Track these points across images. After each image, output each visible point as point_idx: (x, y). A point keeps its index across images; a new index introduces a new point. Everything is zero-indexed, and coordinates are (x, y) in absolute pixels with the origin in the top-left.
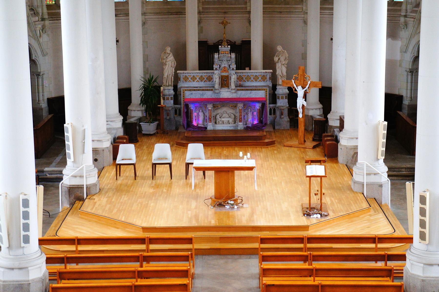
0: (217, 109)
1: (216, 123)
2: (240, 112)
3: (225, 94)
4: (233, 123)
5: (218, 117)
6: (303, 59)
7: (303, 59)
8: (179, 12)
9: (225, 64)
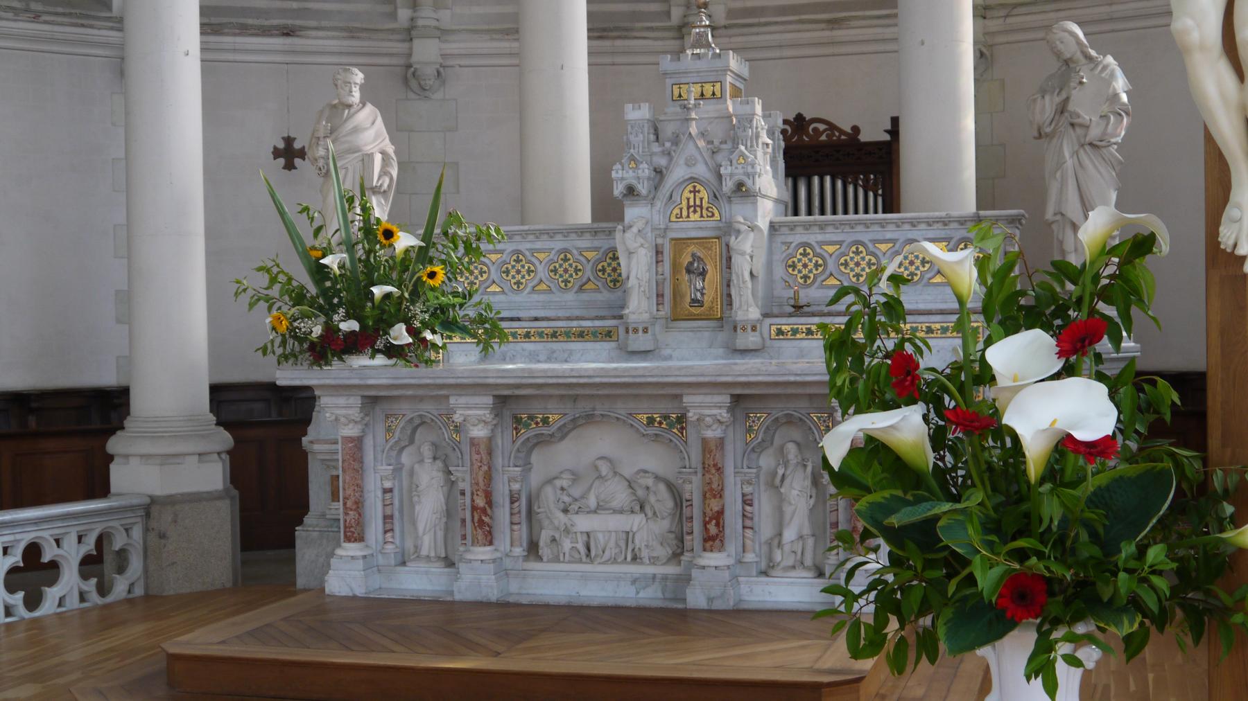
0: (541, 441)
1: (533, 549)
3: (592, 362)
4: (663, 552)
8: (616, 29)
9: (690, 163)
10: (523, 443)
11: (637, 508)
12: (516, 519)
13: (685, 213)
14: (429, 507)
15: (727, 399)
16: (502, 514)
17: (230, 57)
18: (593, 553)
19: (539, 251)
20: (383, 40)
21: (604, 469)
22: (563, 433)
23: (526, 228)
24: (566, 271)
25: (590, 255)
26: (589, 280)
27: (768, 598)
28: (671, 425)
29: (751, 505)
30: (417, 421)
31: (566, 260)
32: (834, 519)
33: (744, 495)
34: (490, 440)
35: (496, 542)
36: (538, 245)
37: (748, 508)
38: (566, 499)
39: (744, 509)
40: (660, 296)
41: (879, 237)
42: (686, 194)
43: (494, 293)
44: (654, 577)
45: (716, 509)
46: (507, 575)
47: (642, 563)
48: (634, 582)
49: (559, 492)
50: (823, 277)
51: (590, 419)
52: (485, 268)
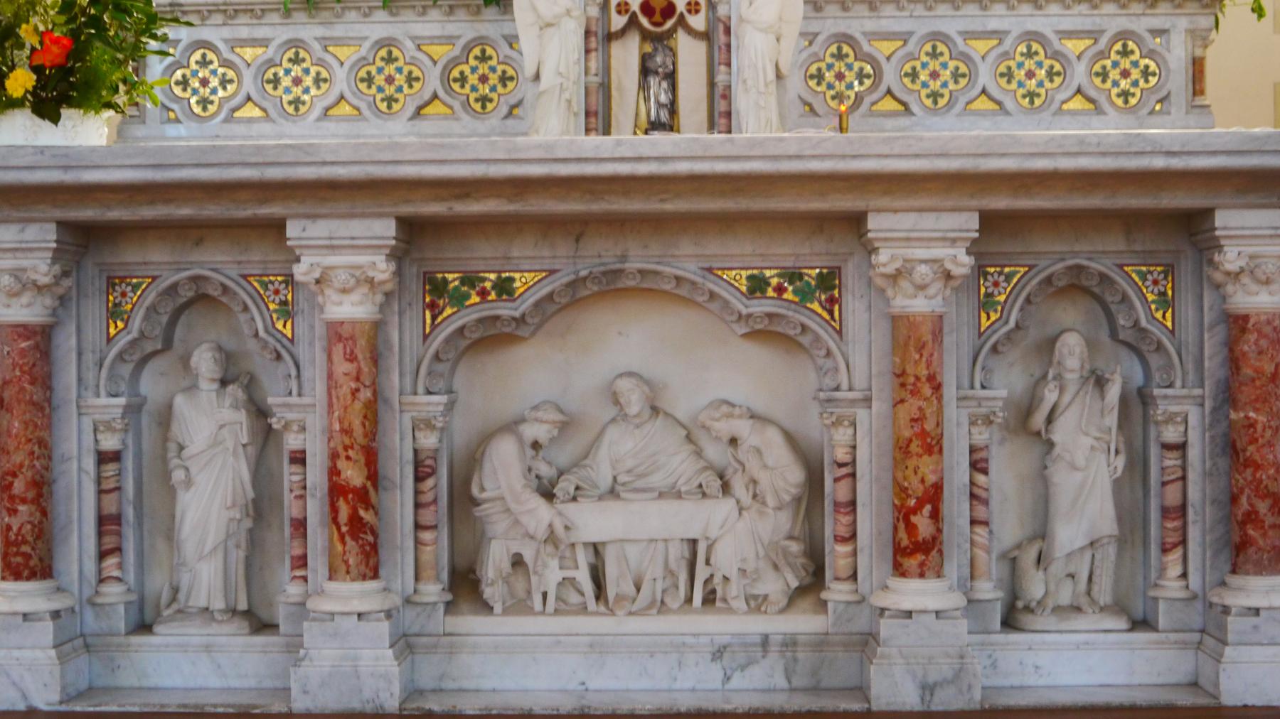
0: (493, 338)
1: (465, 585)
2: (914, 378)
4: (774, 586)
5: (504, 471)
6: (910, 617)
7: (910, 617)
10: (447, 341)
12: (427, 516)
14: (208, 499)
15: (973, 221)
16: (398, 506)
18: (611, 592)
19: (339, 42)
22: (549, 309)
24: (390, 80)
25: (439, 51)
26: (435, 96)
27: (1031, 680)
28: (805, 295)
29: (985, 472)
30: (187, 293)
31: (390, 59)
32: (1172, 496)
33: (973, 450)
34: (377, 327)
35: (382, 572)
37: (981, 479)
39: (972, 483)
41: (976, 25)
43: (250, 120)
44: (765, 641)
45: (931, 478)
47: (730, 611)
48: (719, 654)
50: (875, 96)
51: (610, 287)
52: (231, 74)
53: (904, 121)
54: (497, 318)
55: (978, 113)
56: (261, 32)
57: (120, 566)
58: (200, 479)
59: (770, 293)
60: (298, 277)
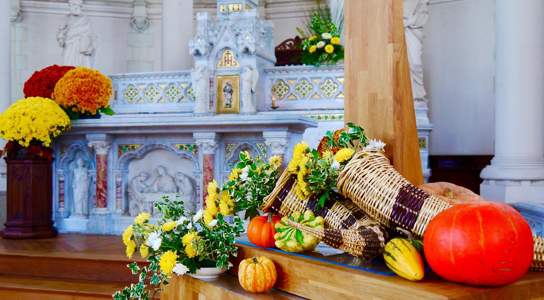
0: (133, 158)
11: (175, 190)
12: (119, 195)
13: (224, 64)
16: (112, 193)
17: (52, 11)
20: (121, 6)
21: (161, 171)
23: (155, 73)
34: (107, 156)
35: (108, 206)
36: (161, 81)
38: (143, 186)
40: (211, 102)
41: (314, 76)
42: (224, 54)
46: (113, 222)
49: (139, 183)
50: (288, 95)
53: (295, 101)
54: (131, 154)
55: (315, 99)
56: (143, 82)
57: (63, 204)
58: (78, 187)
59: (184, 149)
60: (266, 144)
